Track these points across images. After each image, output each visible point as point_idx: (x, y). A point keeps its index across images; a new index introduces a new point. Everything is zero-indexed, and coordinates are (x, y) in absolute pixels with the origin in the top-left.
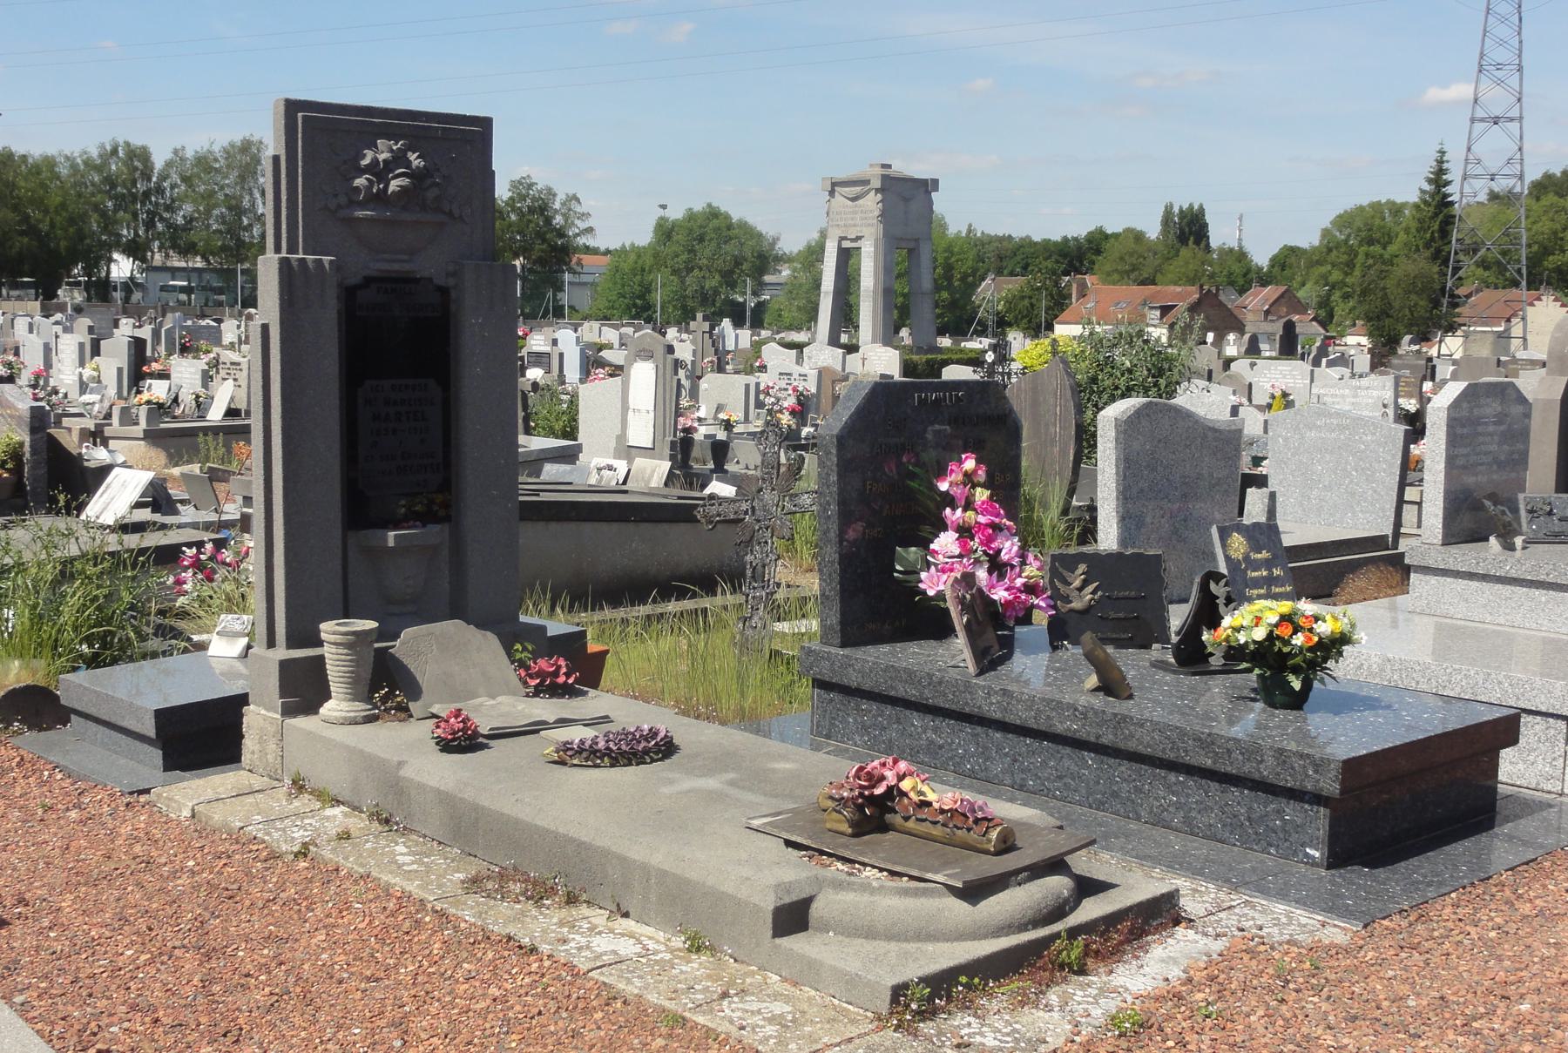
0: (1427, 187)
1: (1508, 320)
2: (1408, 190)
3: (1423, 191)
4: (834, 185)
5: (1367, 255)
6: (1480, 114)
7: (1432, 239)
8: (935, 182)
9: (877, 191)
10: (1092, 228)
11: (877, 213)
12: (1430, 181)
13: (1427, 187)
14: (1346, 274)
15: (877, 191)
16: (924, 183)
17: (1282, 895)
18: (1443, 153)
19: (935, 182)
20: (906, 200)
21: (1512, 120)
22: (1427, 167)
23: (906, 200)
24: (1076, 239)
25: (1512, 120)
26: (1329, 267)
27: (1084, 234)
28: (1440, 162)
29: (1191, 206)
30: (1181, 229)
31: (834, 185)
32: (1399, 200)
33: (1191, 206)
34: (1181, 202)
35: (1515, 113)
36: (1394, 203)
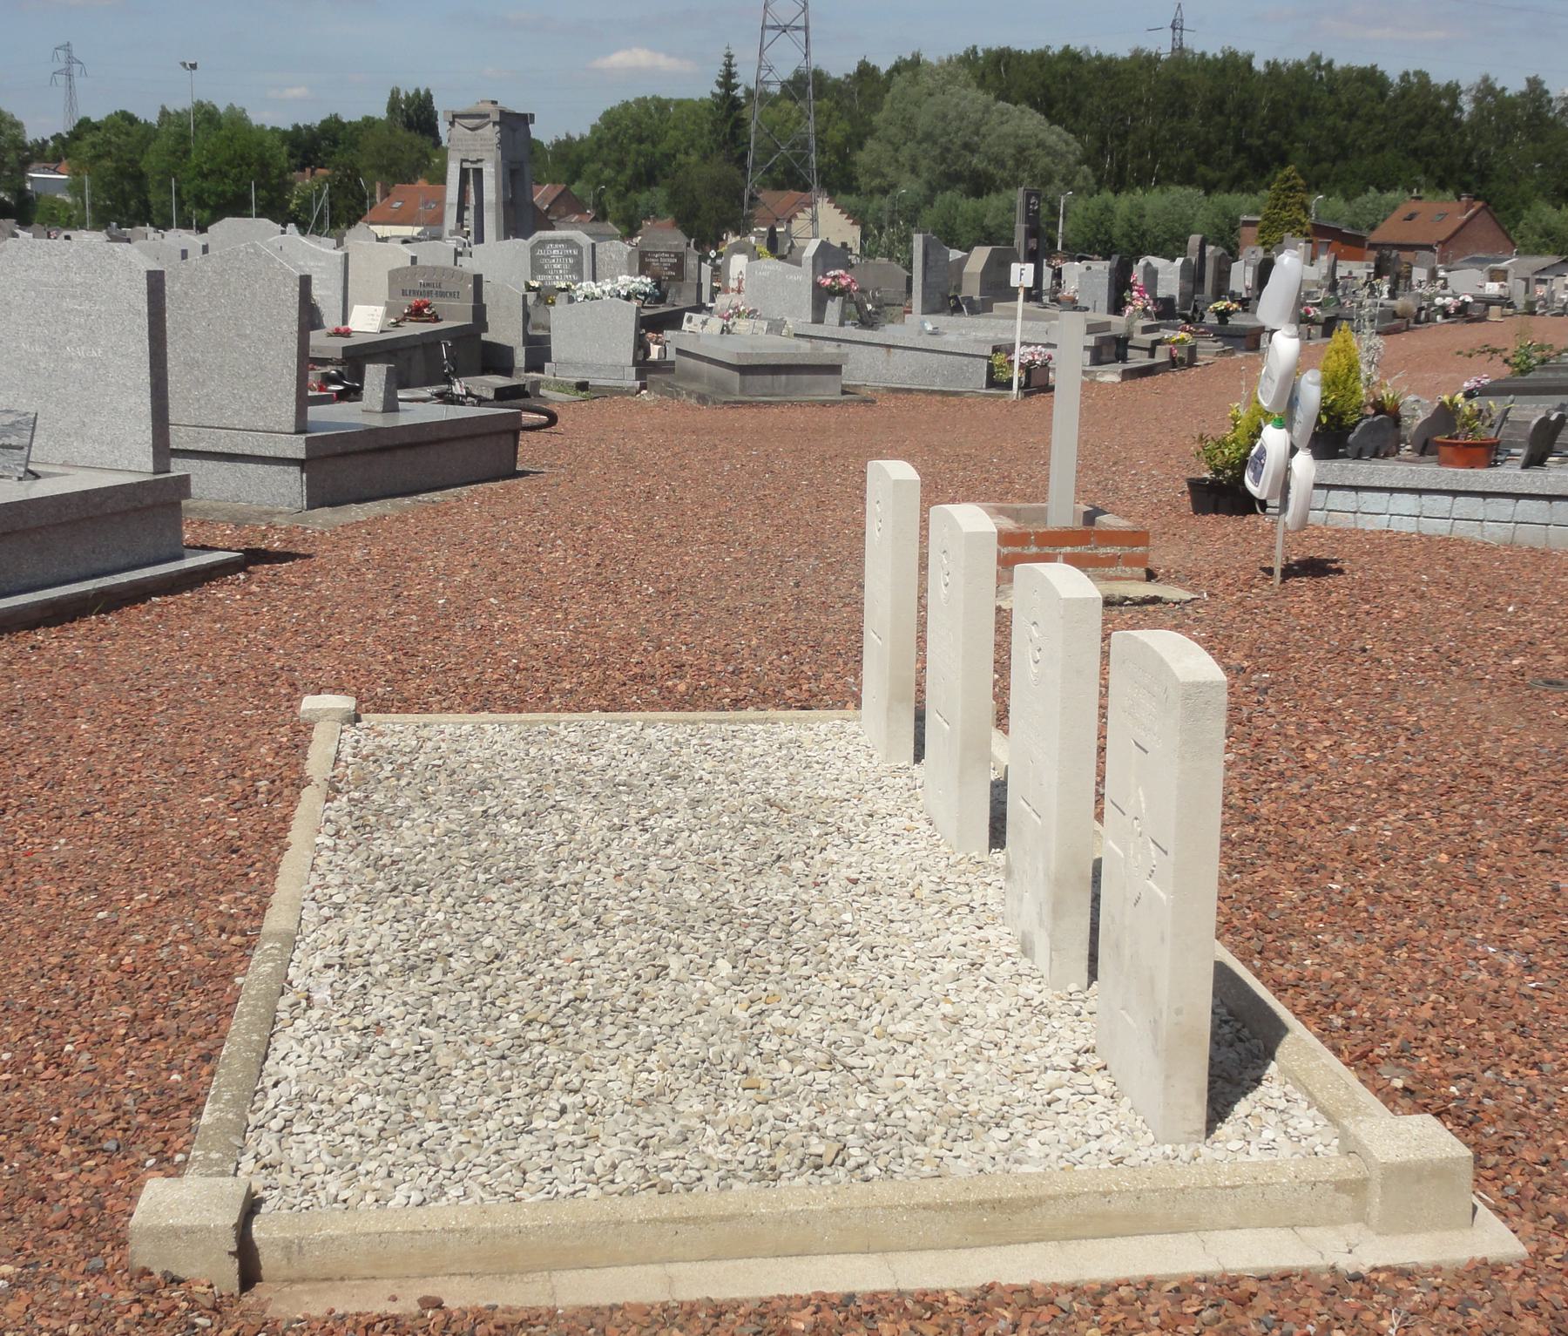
0: (717, 90)
1: (789, 221)
2: (703, 88)
3: (714, 95)
4: (454, 116)
5: (639, 153)
6: (770, 22)
7: (725, 143)
8: (532, 116)
9: (495, 123)
10: (325, 116)
11: (496, 141)
12: (720, 85)
13: (717, 90)
14: (618, 172)
15: (495, 123)
16: (525, 116)
17: (1485, 549)
18: (730, 56)
19: (532, 116)
20: (514, 130)
21: (797, 28)
22: (717, 69)
23: (514, 130)
24: (308, 128)
25: (797, 28)
26: (600, 165)
27: (317, 123)
28: (729, 65)
29: (417, 91)
30: (408, 116)
31: (454, 116)
32: (664, 96)
33: (417, 91)
34: (407, 89)
35: (800, 22)
36: (659, 100)
